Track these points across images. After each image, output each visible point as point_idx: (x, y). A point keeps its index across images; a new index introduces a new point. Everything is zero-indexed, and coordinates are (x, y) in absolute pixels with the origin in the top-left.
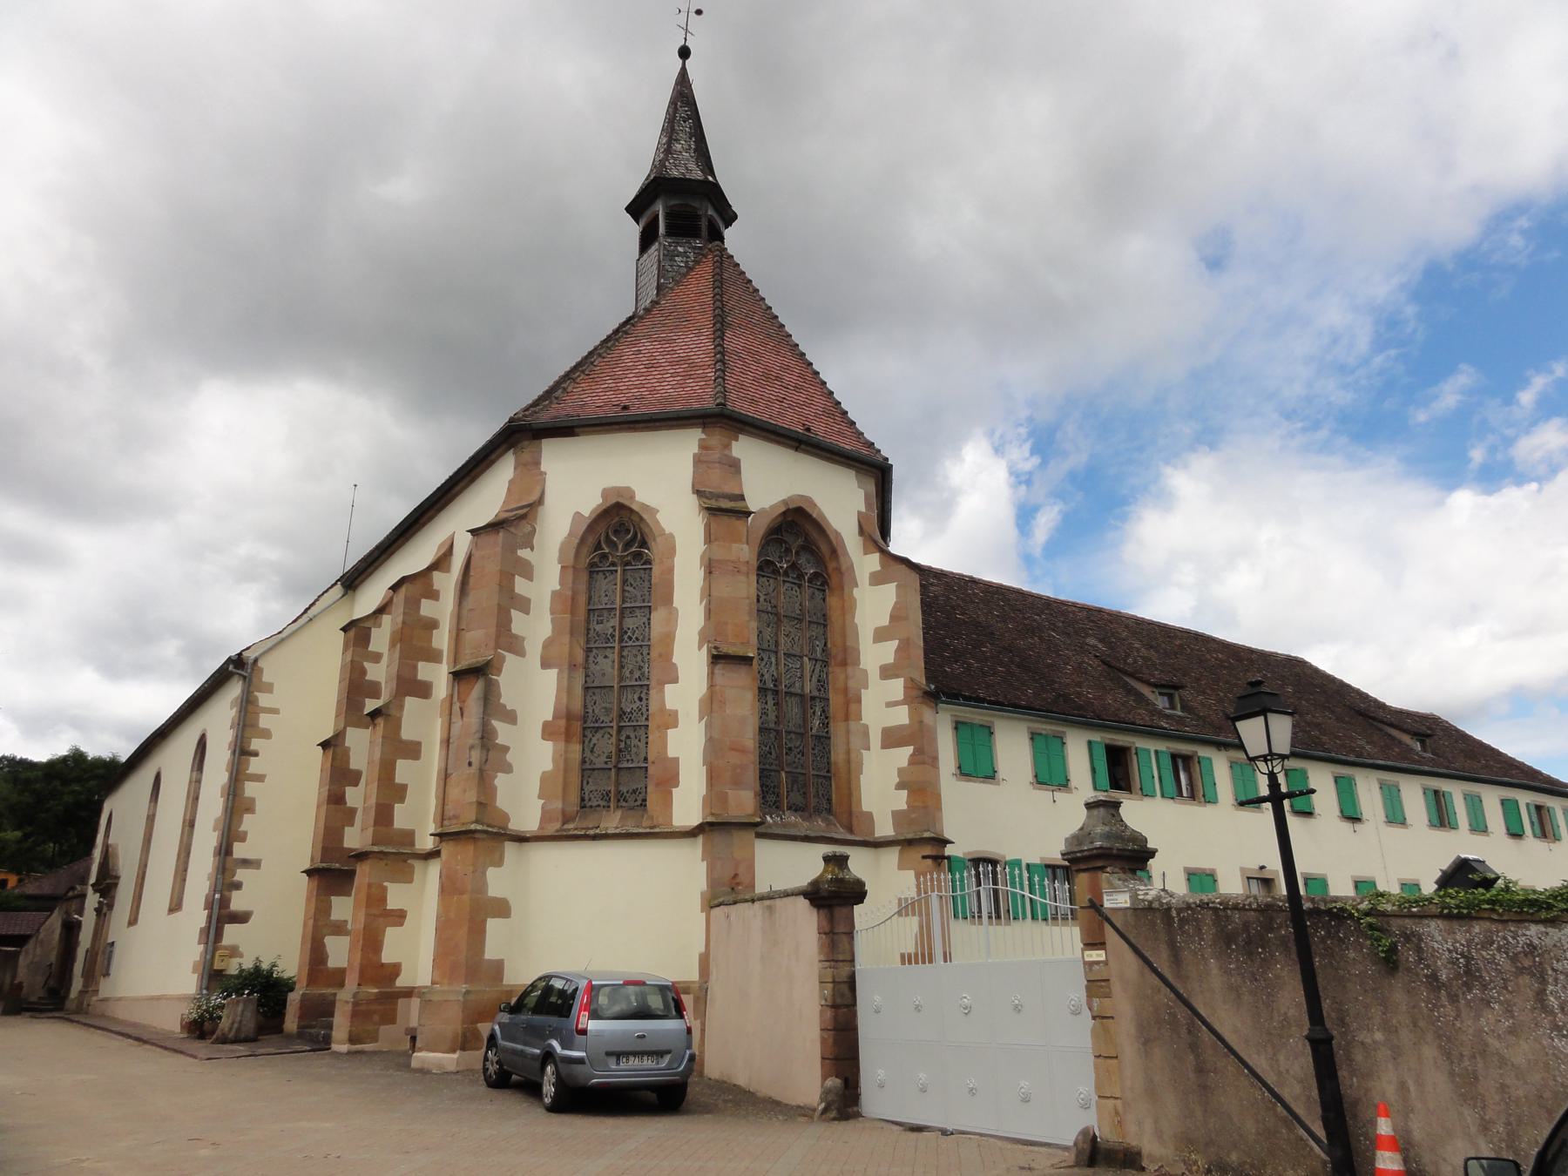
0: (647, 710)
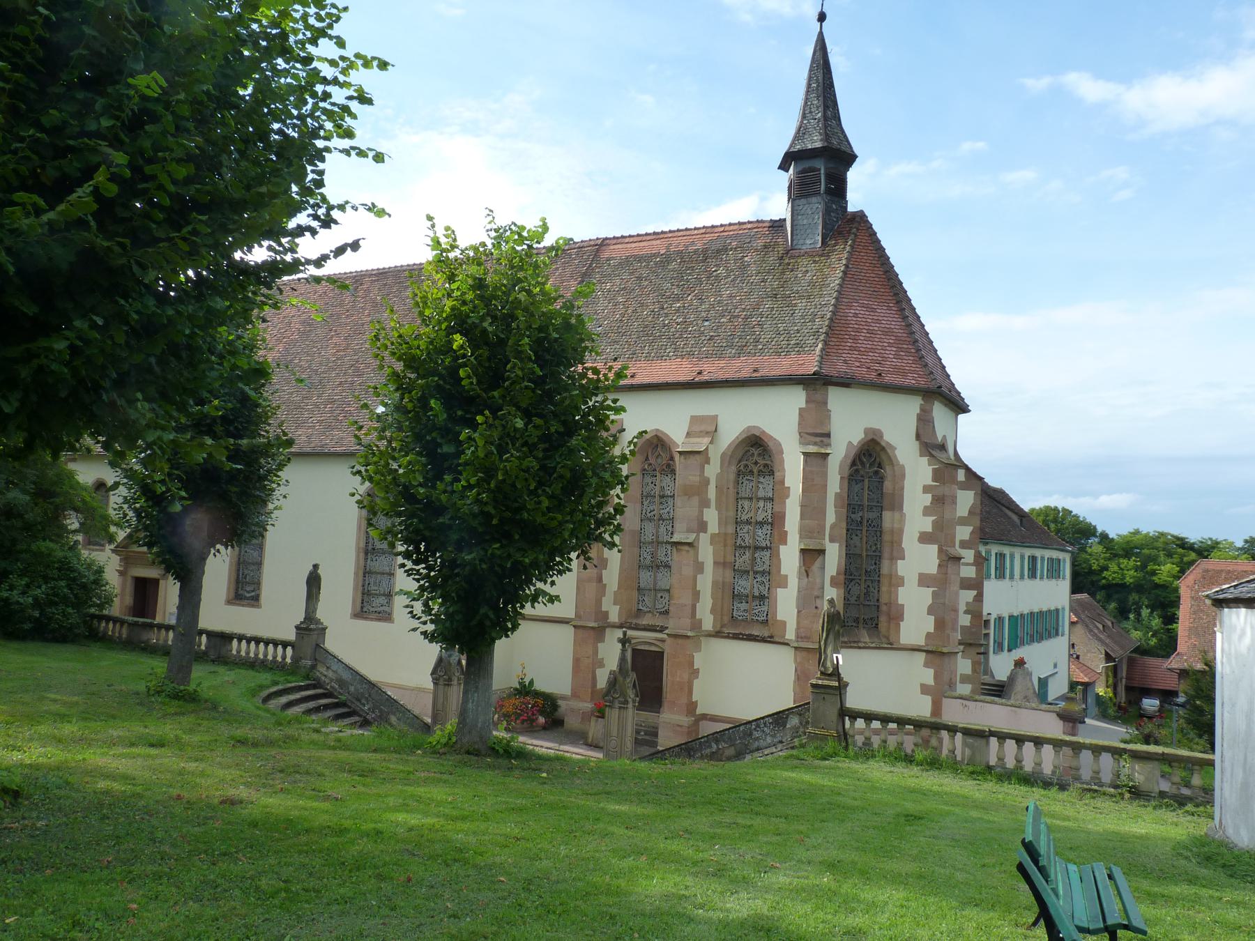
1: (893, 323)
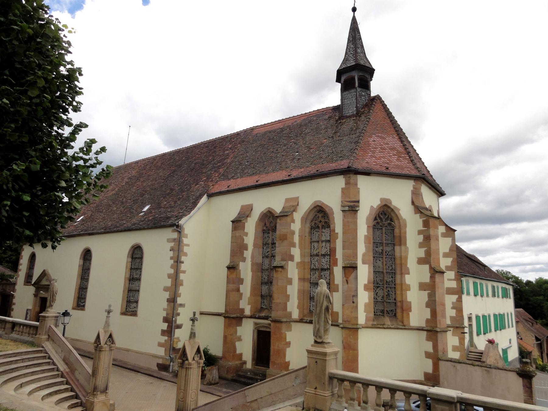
0: (395, 282)
1: (395, 144)
